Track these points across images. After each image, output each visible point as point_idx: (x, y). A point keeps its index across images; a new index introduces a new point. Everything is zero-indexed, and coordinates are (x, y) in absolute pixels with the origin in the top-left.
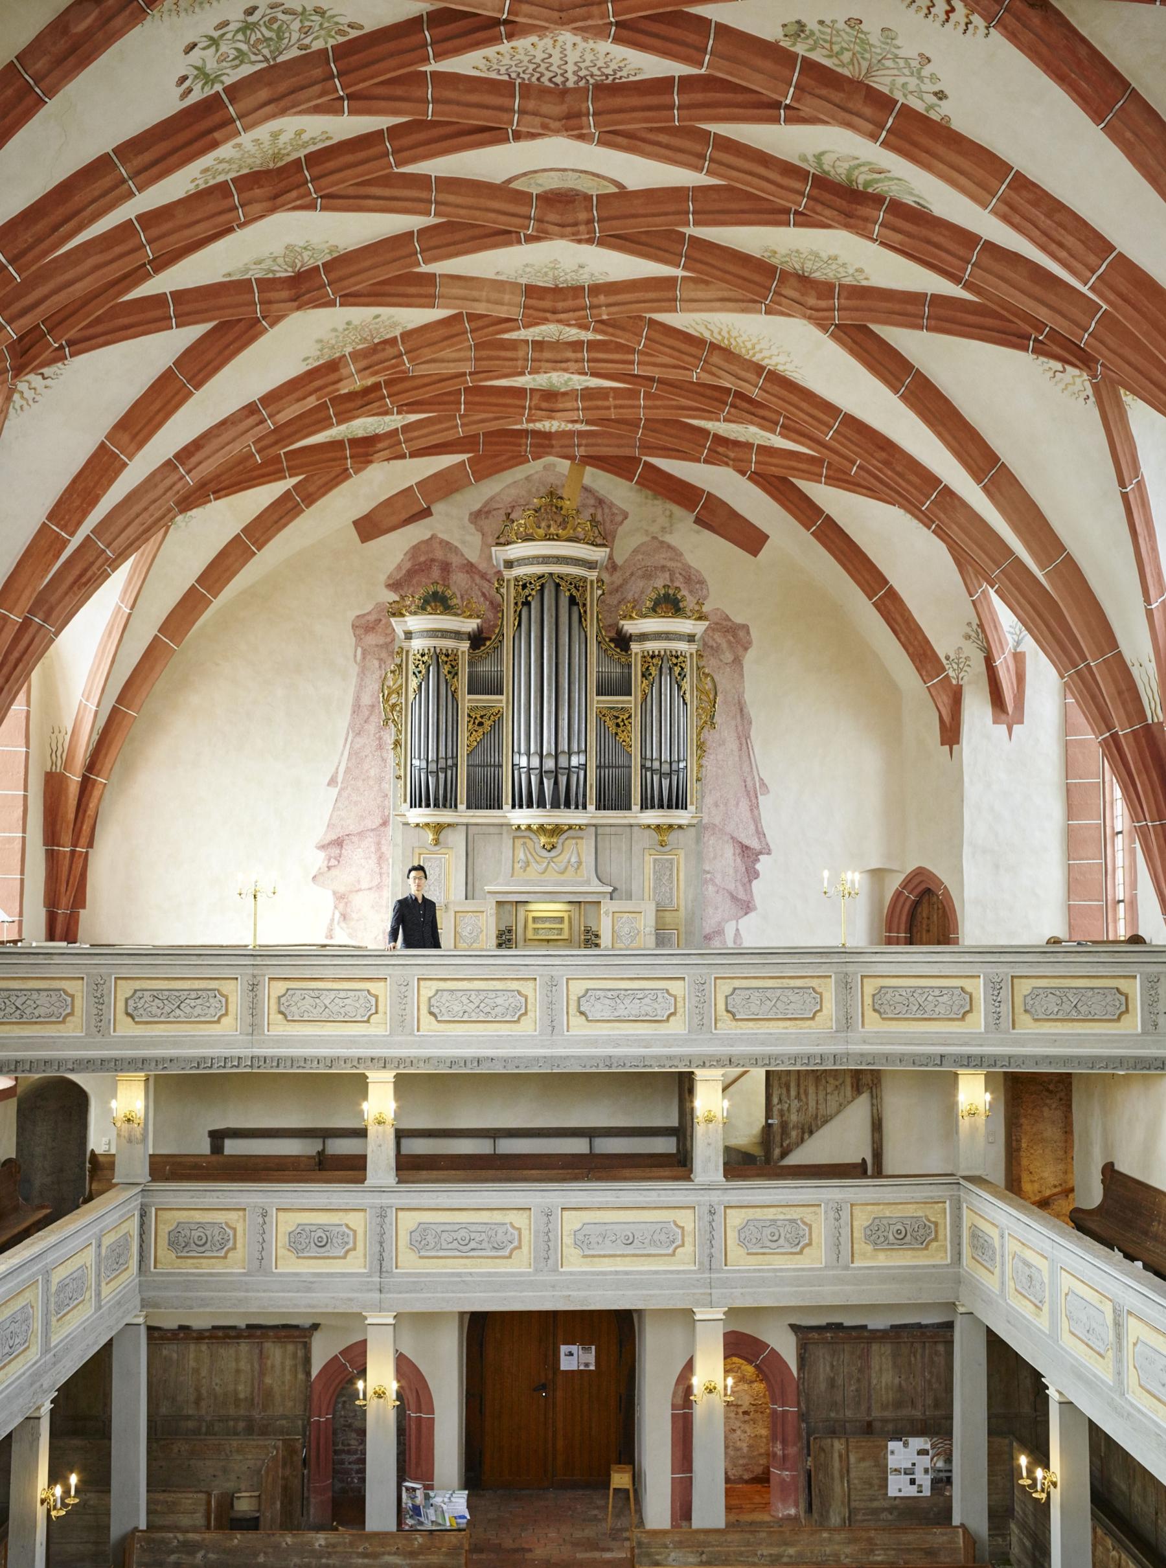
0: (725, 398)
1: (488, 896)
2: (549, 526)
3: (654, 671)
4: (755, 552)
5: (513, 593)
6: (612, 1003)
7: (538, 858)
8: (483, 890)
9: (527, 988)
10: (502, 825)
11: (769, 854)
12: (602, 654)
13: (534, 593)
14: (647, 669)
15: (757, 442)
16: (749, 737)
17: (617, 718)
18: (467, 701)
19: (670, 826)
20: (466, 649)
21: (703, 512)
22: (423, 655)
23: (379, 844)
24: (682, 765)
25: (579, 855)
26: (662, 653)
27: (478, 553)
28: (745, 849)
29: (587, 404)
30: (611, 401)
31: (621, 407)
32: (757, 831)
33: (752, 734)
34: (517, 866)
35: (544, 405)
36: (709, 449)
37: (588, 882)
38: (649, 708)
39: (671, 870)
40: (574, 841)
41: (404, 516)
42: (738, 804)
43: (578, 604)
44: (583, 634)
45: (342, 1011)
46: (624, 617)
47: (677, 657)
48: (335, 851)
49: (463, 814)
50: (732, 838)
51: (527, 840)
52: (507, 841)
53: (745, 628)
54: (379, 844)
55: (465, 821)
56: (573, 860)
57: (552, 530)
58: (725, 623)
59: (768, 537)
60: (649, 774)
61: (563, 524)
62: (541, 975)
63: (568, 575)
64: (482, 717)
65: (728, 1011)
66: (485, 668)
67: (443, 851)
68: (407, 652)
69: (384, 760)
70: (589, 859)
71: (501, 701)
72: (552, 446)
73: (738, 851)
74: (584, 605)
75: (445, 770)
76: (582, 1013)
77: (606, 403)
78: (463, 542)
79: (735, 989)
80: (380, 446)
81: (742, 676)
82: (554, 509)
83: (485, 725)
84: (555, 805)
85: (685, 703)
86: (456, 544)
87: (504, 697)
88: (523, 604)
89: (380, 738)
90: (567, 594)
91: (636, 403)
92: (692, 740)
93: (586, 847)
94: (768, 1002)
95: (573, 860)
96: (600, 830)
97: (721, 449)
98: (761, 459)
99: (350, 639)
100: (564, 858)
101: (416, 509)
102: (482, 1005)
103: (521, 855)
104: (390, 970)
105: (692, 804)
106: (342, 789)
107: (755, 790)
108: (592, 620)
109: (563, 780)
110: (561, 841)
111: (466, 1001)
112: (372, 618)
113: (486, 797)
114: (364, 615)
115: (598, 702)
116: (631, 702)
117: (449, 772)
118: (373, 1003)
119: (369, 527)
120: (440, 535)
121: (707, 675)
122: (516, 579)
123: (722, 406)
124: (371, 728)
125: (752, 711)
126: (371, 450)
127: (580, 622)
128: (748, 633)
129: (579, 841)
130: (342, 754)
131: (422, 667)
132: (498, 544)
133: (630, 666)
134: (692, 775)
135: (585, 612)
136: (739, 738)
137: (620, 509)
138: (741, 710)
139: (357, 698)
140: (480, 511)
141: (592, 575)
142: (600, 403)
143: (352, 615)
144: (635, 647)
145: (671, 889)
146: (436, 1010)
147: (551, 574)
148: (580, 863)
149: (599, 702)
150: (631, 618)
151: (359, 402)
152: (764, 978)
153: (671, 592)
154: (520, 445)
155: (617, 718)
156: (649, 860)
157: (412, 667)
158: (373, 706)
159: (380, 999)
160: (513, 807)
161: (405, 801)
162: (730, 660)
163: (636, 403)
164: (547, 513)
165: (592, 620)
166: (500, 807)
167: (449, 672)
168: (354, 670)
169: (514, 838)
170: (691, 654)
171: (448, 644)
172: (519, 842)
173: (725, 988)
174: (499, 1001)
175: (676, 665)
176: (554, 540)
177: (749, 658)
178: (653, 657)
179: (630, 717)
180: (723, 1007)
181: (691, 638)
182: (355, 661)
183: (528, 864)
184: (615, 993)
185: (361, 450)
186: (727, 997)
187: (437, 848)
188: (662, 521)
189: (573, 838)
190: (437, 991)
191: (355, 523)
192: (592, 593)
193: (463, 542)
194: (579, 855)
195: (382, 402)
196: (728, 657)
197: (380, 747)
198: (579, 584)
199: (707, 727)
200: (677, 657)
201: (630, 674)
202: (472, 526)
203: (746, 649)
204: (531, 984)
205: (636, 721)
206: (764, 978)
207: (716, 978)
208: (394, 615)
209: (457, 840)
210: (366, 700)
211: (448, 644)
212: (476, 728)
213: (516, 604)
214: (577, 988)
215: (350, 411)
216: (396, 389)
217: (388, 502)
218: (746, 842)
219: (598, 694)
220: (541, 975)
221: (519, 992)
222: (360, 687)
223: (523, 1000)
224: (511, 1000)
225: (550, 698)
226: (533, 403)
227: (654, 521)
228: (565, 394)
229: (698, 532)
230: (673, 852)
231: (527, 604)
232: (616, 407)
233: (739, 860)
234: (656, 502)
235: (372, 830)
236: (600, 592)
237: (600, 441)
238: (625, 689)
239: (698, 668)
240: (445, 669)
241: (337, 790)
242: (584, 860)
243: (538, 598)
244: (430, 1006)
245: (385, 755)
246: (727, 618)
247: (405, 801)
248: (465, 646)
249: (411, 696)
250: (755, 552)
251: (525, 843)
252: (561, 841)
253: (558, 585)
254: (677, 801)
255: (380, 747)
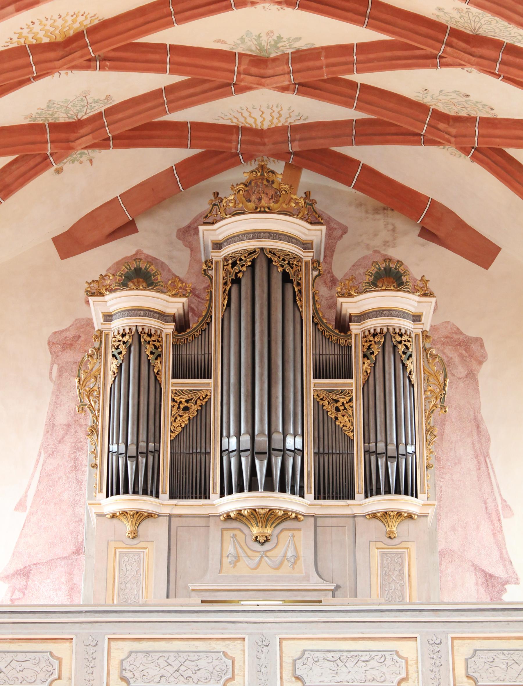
0: (440, 36)
1: (193, 594)
2: (260, 199)
3: (376, 350)
4: (486, 263)
5: (222, 274)
6: (333, 666)
7: (250, 553)
8: (187, 587)
9: (234, 649)
10: (208, 516)
11: (517, 582)
12: (319, 336)
13: (244, 269)
14: (369, 348)
15: (480, 115)
16: (488, 455)
17: (337, 401)
18: (171, 385)
19: (399, 514)
20: (171, 331)
21: (427, 220)
22: (123, 335)
23: (70, 573)
24: (410, 449)
25: (296, 549)
26: (385, 330)
27: (186, 268)
28: (489, 578)
29: (298, 66)
30: (323, 61)
31: (334, 65)
32: (502, 558)
33: (492, 452)
34: (226, 561)
35: (254, 70)
36: (429, 125)
37: (307, 579)
38: (371, 389)
39: (402, 564)
40: (290, 533)
41: (108, 229)
42: (478, 527)
43: (291, 282)
44: (298, 314)
45: (20, 675)
46: (343, 295)
47: (401, 335)
48: (20, 582)
49: (163, 504)
50: (473, 565)
51: (238, 533)
52: (214, 533)
53: (479, 341)
54: (70, 573)
55: (166, 510)
56: (290, 554)
57: (263, 203)
58: (456, 337)
59: (499, 249)
60: (373, 458)
61: (276, 197)
62: (250, 634)
63: (280, 251)
64: (187, 401)
65: (468, 677)
66: (192, 351)
67: (143, 545)
68: (107, 335)
69: (79, 482)
70: (307, 553)
71: (209, 385)
72: (264, 144)
73: (481, 580)
74: (299, 284)
75: (146, 454)
76: (298, 678)
77: (318, 63)
78: (171, 258)
79: (476, 651)
80: (82, 131)
81: (477, 390)
82: (265, 182)
83: (191, 410)
84: (269, 487)
85: (412, 385)
86: (162, 259)
87: (211, 381)
88: (233, 282)
89: (76, 459)
90: (280, 269)
91: (349, 59)
92: (420, 424)
93: (303, 538)
94: (515, 666)
95: (290, 554)
96: (320, 522)
97: (442, 126)
98: (485, 131)
99: (45, 356)
100: (278, 553)
101: (120, 222)
102: (183, 668)
103: (230, 549)
104: (76, 628)
105: (423, 492)
106: (31, 514)
107: (497, 511)
108: (307, 302)
109: (277, 463)
110: (276, 533)
111: (163, 664)
112: (70, 334)
113: (190, 485)
114: (62, 331)
115: (315, 385)
116: (353, 385)
117: (151, 458)
118: (56, 666)
119: (70, 243)
120: (146, 251)
121: (434, 357)
122: (226, 259)
123: (438, 45)
124: (66, 448)
125: (490, 427)
126: (73, 136)
127: (295, 301)
128: (482, 346)
129: (295, 533)
130: (33, 475)
131: (123, 349)
132: (205, 223)
133: (349, 348)
134: (421, 463)
135: (300, 292)
136: (477, 456)
137: (339, 223)
138: (478, 427)
139: (52, 417)
140: (189, 227)
141: (307, 256)
142: (311, 64)
143: (47, 332)
144: (355, 328)
145: (402, 586)
146: (128, 675)
147: (262, 249)
148: (297, 558)
149: (314, 386)
150: (350, 295)
151: (60, 53)
152: (509, 638)
153: (393, 266)
154: (230, 142)
155: (337, 401)
156: (376, 553)
157: (111, 350)
158: (69, 425)
159: (64, 662)
160: (222, 495)
161: (101, 491)
162: (463, 375)
163: (349, 59)
164: (258, 186)
165: (307, 302)
166: (207, 497)
167: (152, 353)
168: (49, 387)
169: (222, 530)
170: (417, 335)
171: (153, 323)
172: (228, 535)
173: (464, 650)
174: (202, 663)
175: (400, 342)
176: (265, 212)
177: (484, 373)
178: (374, 335)
179: (351, 400)
180: (463, 672)
181: (417, 318)
182: (51, 378)
183: (237, 559)
184: (337, 655)
185: (63, 136)
186: (467, 660)
187: (135, 541)
188: (385, 235)
189: (290, 530)
190: (131, 653)
191: (55, 240)
192: (307, 274)
193: (171, 258)
194: (296, 549)
195: (84, 51)
196: (461, 371)
197: (75, 468)
198: (291, 260)
199: (437, 410)
200: (401, 335)
201: (350, 356)
202: (181, 242)
203: (481, 363)
204: (238, 644)
205: (358, 406)
206: (509, 638)
207: (453, 639)
208: (93, 294)
209: (156, 531)
210: (62, 418)
211: (153, 323)
212: (181, 412)
213: (225, 284)
214: (292, 649)
215: (51, 61)
216: (98, 36)
217: (91, 217)
218: (491, 570)
219: (315, 377)
220: (250, 634)
221: (225, 654)
222: (56, 404)
223: (230, 662)
224: (216, 662)
225: (262, 375)
226: (242, 68)
227: (376, 235)
228: (275, 59)
229: (423, 245)
230: (403, 545)
231: (237, 281)
232: (328, 66)
233: (482, 590)
234: (378, 216)
235: (64, 558)
236: (316, 273)
237: (314, 134)
238: (346, 372)
239: (425, 350)
240: (148, 349)
241: (24, 515)
242: (301, 553)
243: (248, 275)
244: (122, 669)
245: (80, 477)
246: (458, 331)
247: (101, 491)
248: (170, 328)
249: (110, 379)
250: (486, 263)
251: (234, 536)
252: (276, 533)
253: (270, 261)
254: (408, 488)
255: (75, 468)
